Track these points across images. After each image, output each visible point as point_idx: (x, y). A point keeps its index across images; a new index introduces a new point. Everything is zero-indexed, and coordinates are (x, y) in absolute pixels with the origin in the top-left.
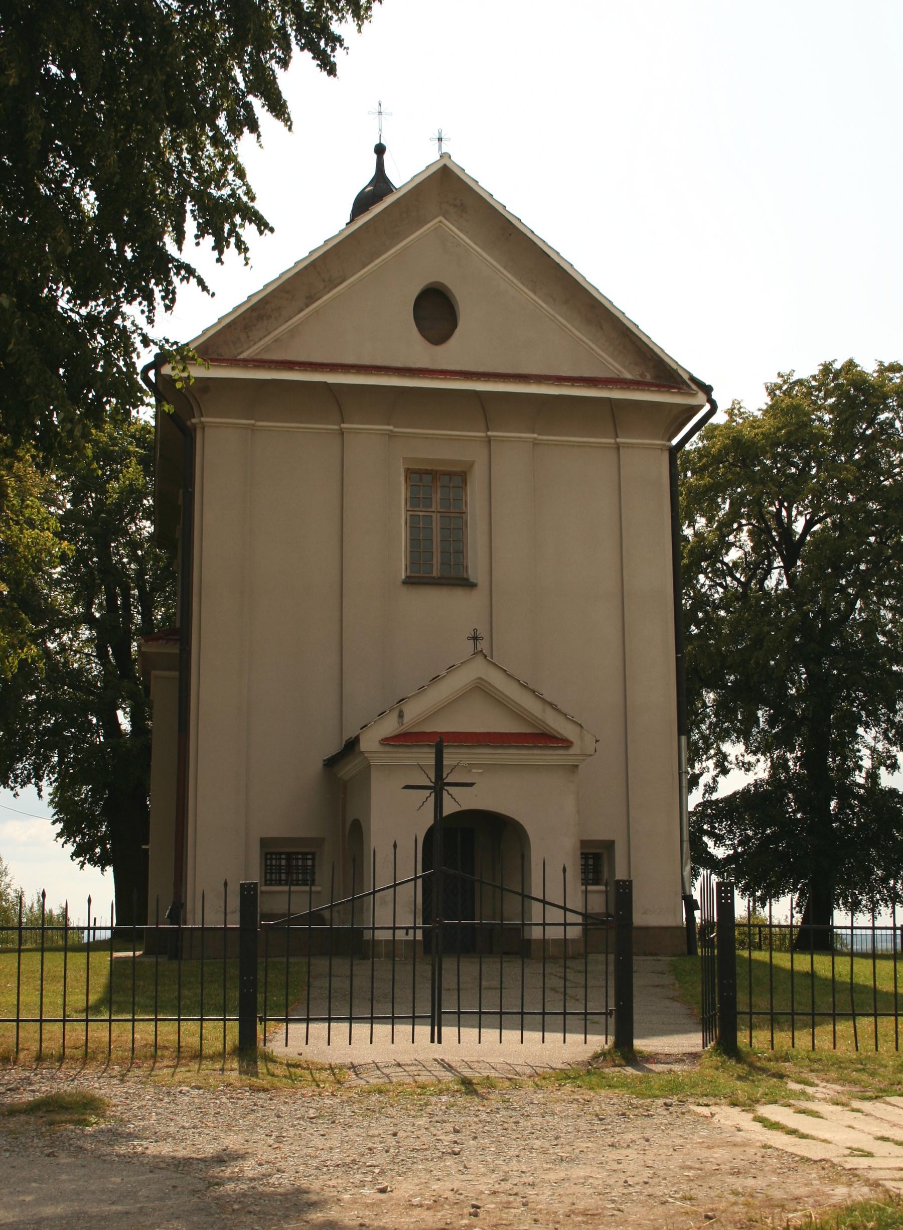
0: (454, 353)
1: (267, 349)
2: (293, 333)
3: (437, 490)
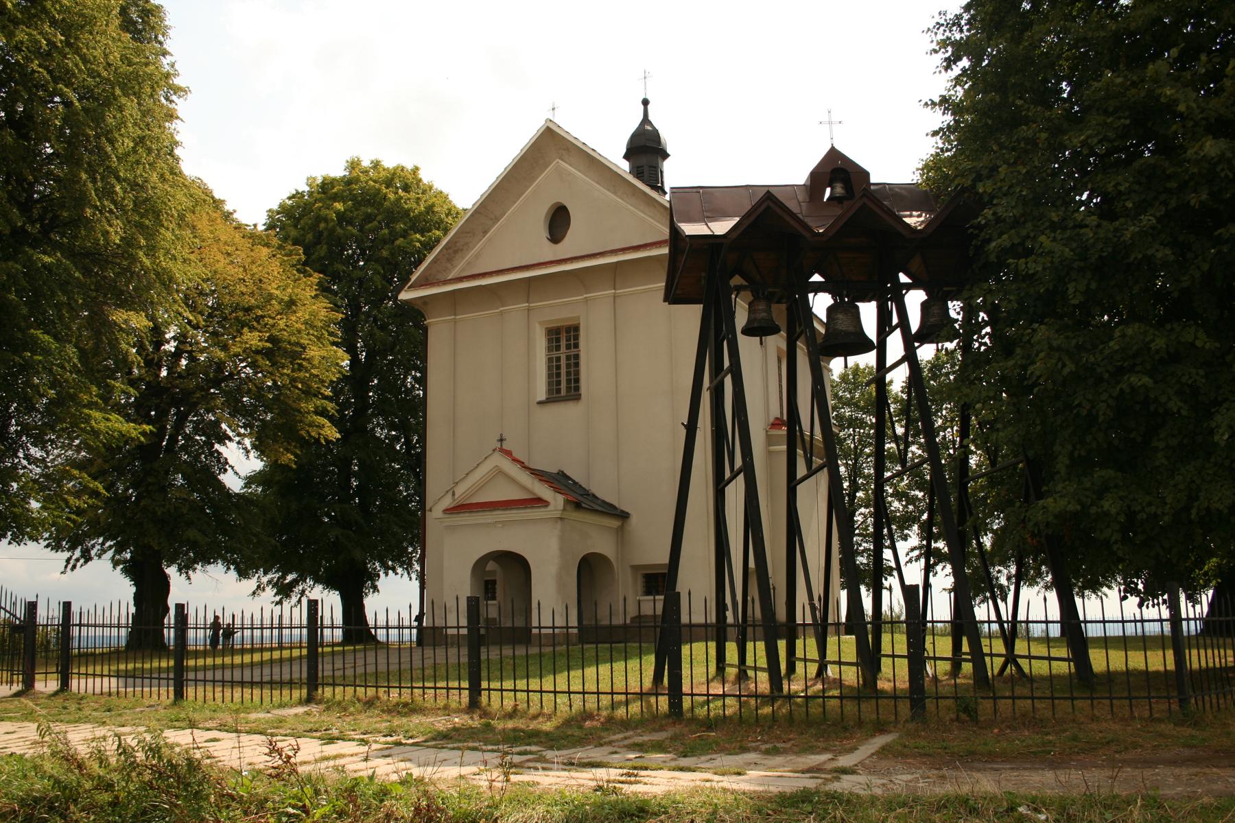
0: (573, 243)
1: (463, 270)
2: (477, 256)
3: (564, 338)
